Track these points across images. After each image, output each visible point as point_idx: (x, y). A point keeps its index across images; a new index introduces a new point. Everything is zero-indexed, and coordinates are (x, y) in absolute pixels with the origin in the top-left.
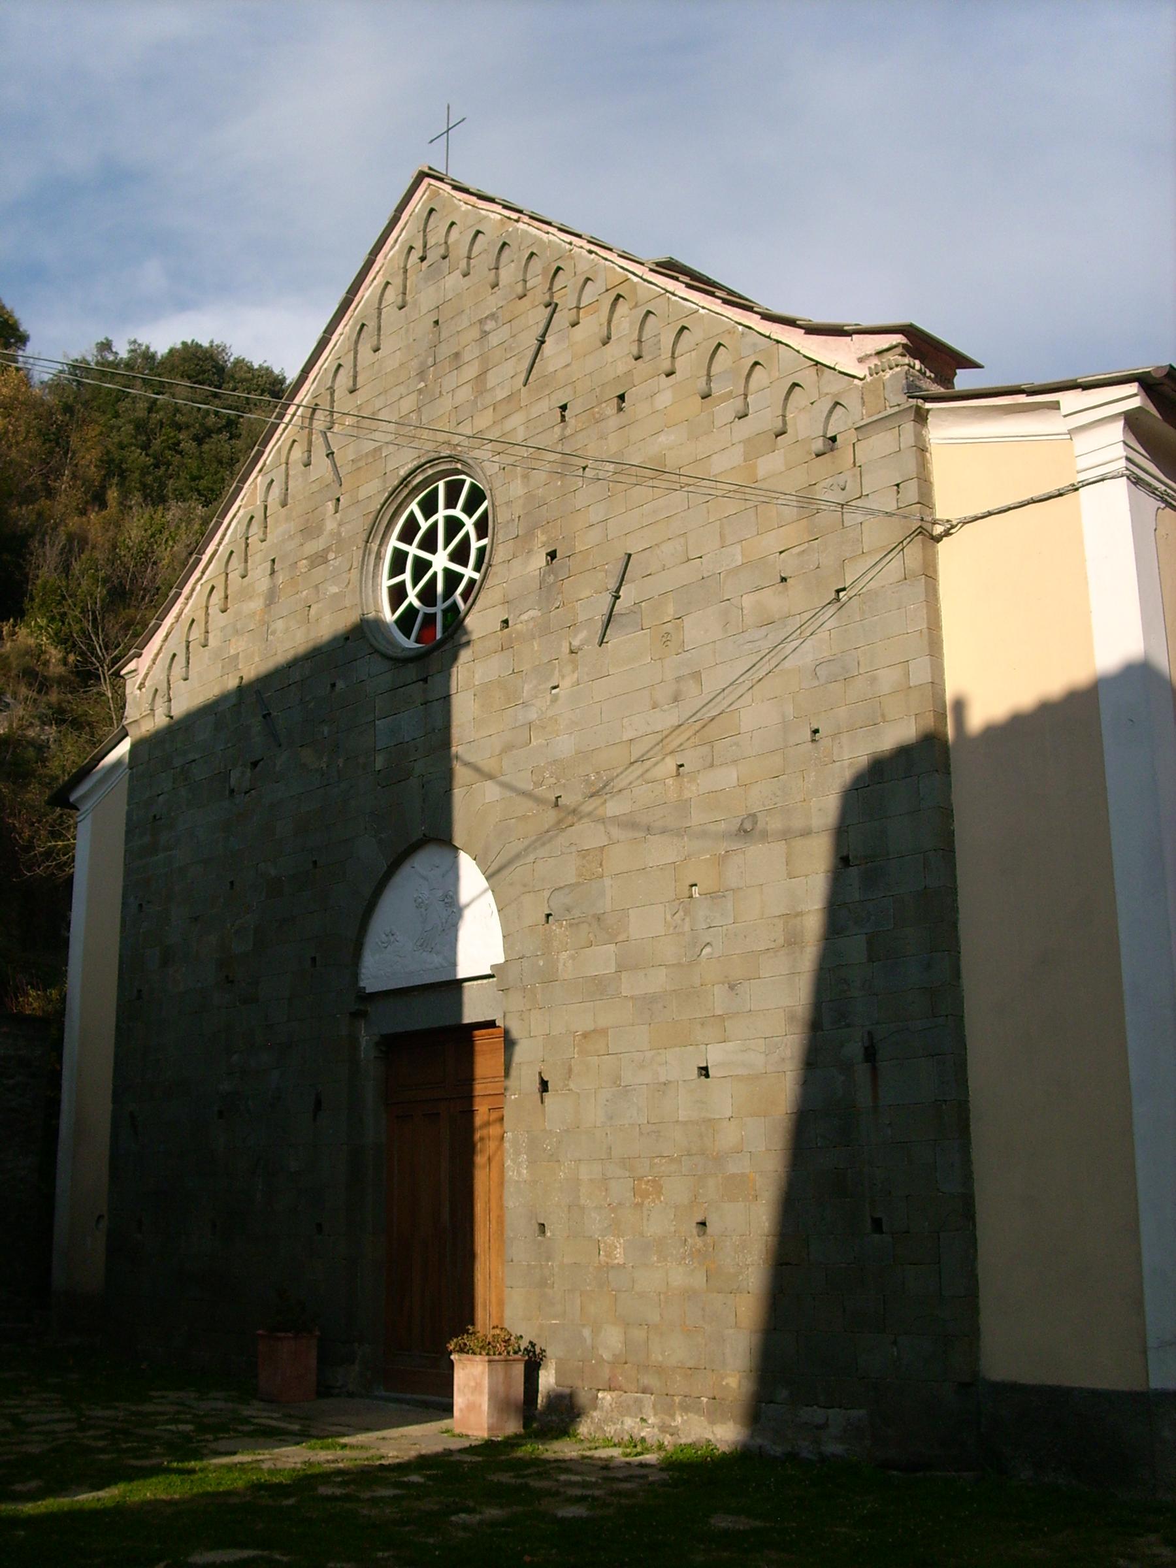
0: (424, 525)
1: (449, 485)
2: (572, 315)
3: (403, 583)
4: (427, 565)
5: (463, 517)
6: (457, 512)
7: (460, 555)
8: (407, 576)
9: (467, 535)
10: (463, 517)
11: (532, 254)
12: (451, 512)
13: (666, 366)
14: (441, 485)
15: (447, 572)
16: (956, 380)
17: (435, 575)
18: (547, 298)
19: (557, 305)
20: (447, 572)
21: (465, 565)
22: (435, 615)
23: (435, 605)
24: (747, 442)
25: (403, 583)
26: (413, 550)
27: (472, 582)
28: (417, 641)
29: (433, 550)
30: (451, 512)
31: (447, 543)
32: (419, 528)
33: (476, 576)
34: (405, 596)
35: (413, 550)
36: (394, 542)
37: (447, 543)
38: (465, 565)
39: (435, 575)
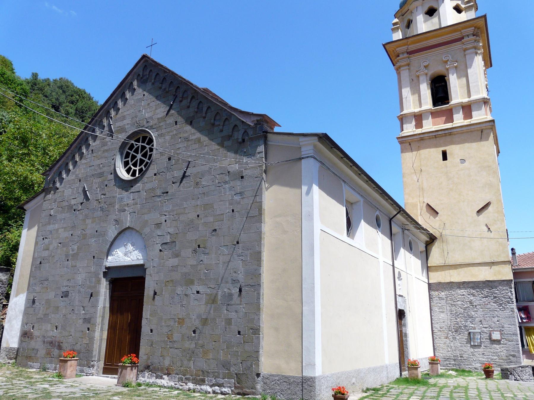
0: (143, 166)
1: (143, 137)
2: (181, 99)
3: (128, 161)
4: (136, 157)
5: (132, 167)
6: (133, 168)
7: (134, 157)
8: (130, 159)
9: (147, 151)
10: (132, 167)
11: (172, 82)
12: (135, 168)
13: (204, 115)
14: (137, 175)
15: (141, 159)
16: (274, 129)
17: (141, 153)
18: (174, 93)
19: (177, 96)
20: (141, 159)
21: (132, 154)
22: (136, 170)
23: (137, 167)
24: (222, 137)
25: (128, 161)
26: (132, 152)
27: (147, 163)
28: (131, 176)
29: (138, 153)
30: (135, 168)
31: (137, 160)
32: (134, 147)
33: (148, 161)
34: (129, 164)
35: (132, 152)
36: (127, 150)
37: (137, 160)
38: (146, 158)
39: (141, 153)
